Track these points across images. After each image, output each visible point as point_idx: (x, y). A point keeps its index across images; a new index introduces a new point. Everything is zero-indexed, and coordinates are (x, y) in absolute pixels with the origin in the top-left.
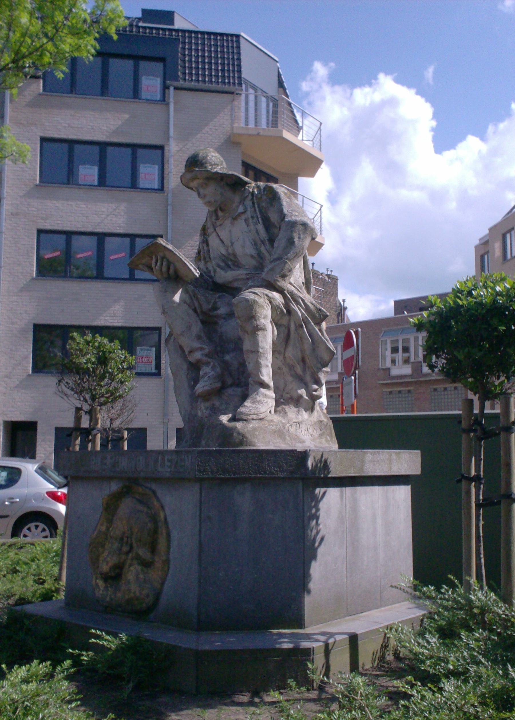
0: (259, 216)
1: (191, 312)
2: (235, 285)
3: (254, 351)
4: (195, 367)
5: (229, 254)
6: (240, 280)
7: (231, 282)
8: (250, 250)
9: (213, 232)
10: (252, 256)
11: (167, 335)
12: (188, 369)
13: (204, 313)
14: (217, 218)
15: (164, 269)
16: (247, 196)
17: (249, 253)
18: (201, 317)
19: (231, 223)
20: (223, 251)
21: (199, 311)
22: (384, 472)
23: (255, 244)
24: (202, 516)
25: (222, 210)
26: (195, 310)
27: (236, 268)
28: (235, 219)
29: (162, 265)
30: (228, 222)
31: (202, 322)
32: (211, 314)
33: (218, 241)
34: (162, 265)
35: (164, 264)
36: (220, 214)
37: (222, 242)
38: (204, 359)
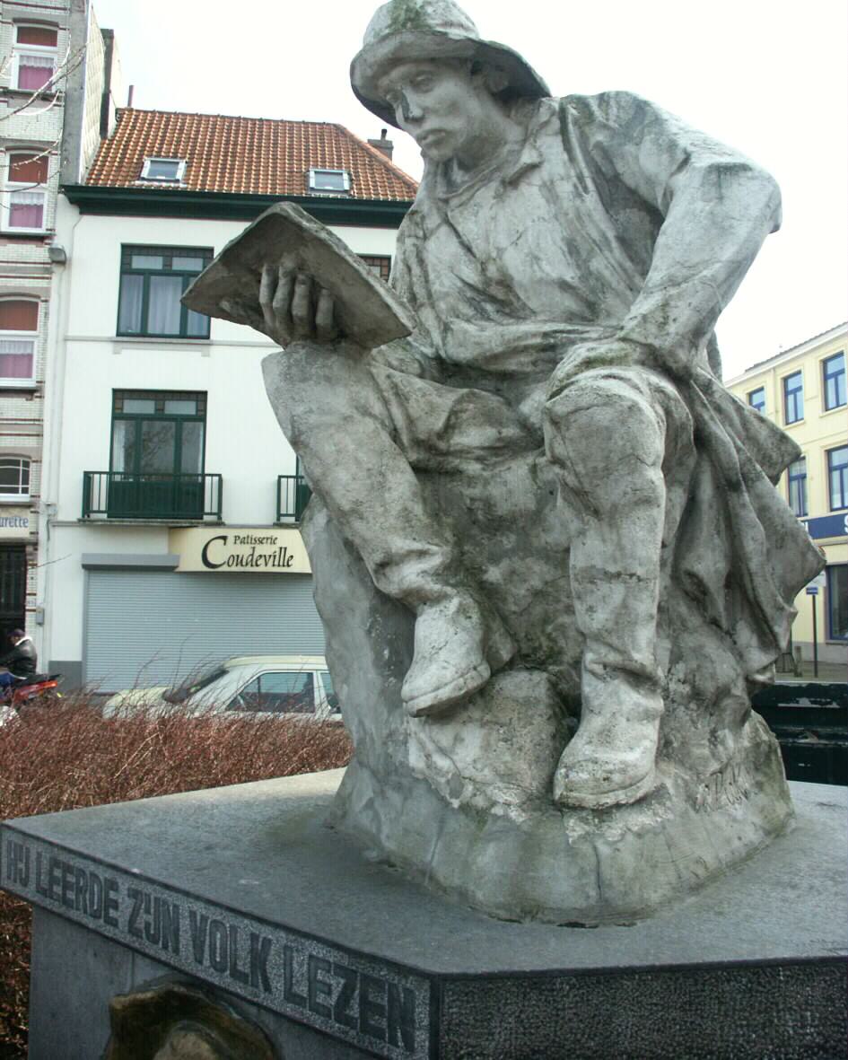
0: (586, 173)
1: (385, 438)
2: (512, 365)
3: (618, 575)
4: (400, 612)
5: (488, 282)
6: (526, 349)
7: (496, 357)
8: (559, 267)
9: (439, 226)
10: (564, 286)
11: (664, 418)
12: (373, 611)
13: (418, 443)
14: (450, 184)
15: (300, 308)
16: (547, 123)
17: (554, 275)
18: (414, 456)
19: (499, 197)
20: (471, 275)
21: (405, 439)
22: (843, 882)
23: (572, 248)
24: (173, 449)
25: (462, 166)
26: (395, 435)
27: (511, 321)
28: (513, 183)
29: (291, 294)
30: (486, 194)
31: (418, 469)
32: (442, 445)
33: (453, 247)
34: (291, 294)
35: (300, 290)
36: (458, 175)
37: (468, 249)
38: (433, 586)
